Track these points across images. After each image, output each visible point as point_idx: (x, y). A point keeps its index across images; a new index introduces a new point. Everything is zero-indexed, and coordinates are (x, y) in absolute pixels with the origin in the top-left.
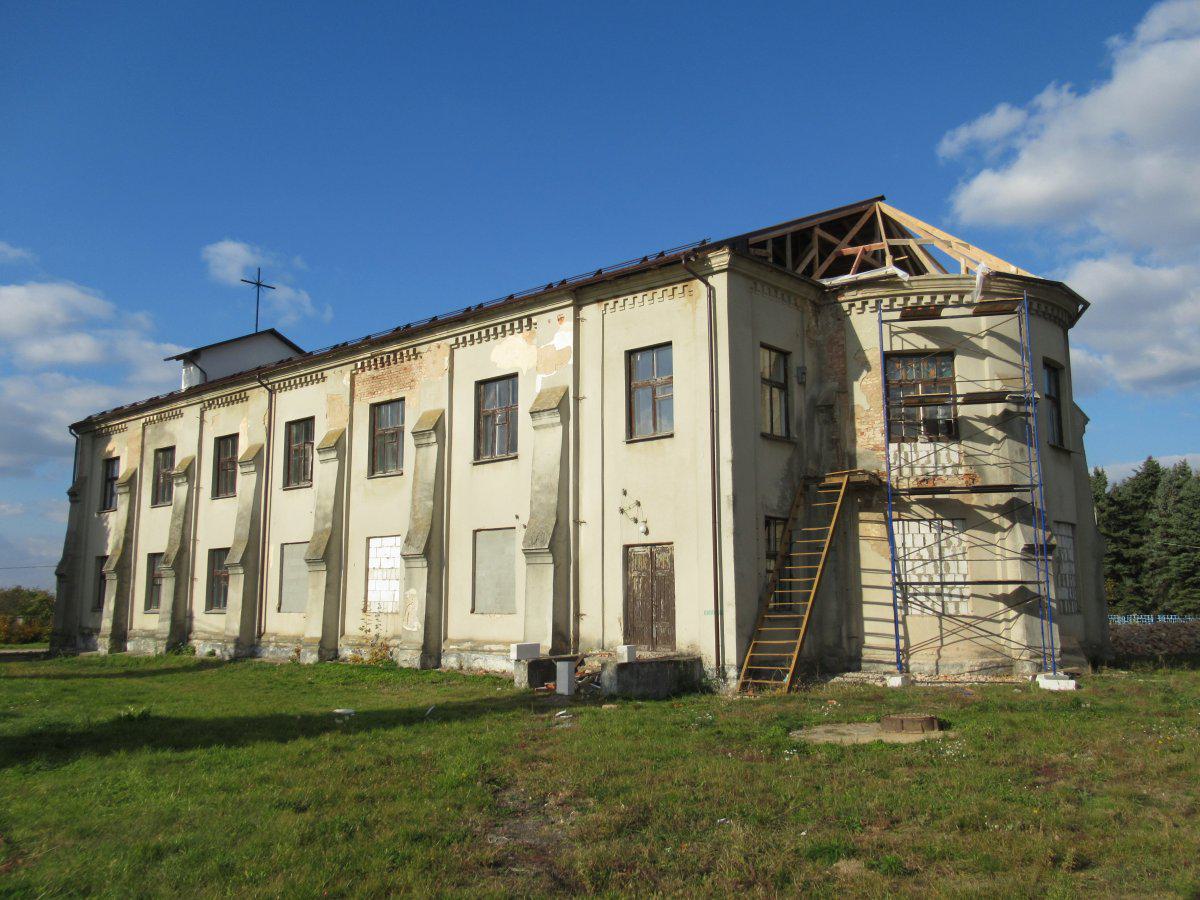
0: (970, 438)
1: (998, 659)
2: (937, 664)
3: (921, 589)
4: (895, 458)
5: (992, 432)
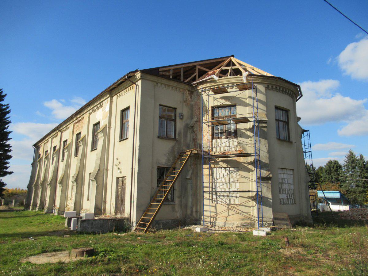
0: (241, 137)
1: (248, 222)
2: (225, 223)
3: (222, 194)
4: (215, 145)
5: (249, 133)
